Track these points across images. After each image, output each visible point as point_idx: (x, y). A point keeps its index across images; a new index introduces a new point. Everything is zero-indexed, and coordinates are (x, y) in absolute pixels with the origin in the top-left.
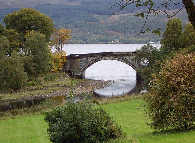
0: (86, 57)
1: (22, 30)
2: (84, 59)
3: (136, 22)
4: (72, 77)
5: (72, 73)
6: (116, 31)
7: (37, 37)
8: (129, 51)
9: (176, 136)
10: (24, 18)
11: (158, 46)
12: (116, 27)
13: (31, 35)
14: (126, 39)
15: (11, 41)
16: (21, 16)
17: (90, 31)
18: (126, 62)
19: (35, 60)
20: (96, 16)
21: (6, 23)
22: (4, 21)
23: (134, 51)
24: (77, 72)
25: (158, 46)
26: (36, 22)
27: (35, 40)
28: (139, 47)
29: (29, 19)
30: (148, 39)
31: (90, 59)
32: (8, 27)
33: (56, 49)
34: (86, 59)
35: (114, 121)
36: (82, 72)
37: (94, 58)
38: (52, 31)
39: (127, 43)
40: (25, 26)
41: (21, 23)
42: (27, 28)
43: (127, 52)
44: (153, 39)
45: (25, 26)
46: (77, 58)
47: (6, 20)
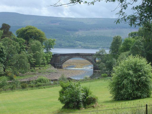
0: (63, 56)
1: (27, 38)
2: (62, 57)
3: (92, 36)
4: (55, 67)
5: (55, 65)
6: (80, 41)
7: (36, 43)
8: (54, 52)
9: (117, 103)
10: (28, 31)
11: (108, 52)
12: (79, 39)
13: (34, 43)
14: (85, 46)
15: (20, 45)
16: (26, 30)
17: (64, 40)
18: (88, 59)
19: (34, 57)
20: (68, 32)
21: (17, 34)
22: (16, 33)
23: (95, 53)
24: (58, 64)
25: (108, 52)
26: (35, 34)
27: (36, 45)
28: (98, 51)
29: (31, 32)
30: (98, 46)
31: (66, 57)
32: (18, 37)
33: (46, 51)
34: (64, 57)
35: (91, 94)
36: (61, 65)
37: (68, 57)
38: (44, 40)
39: (86, 48)
40: (29, 36)
41: (26, 35)
42: (29, 37)
43: (88, 54)
44: (102, 46)
45: (29, 36)
46: (58, 56)
47: (17, 33)
